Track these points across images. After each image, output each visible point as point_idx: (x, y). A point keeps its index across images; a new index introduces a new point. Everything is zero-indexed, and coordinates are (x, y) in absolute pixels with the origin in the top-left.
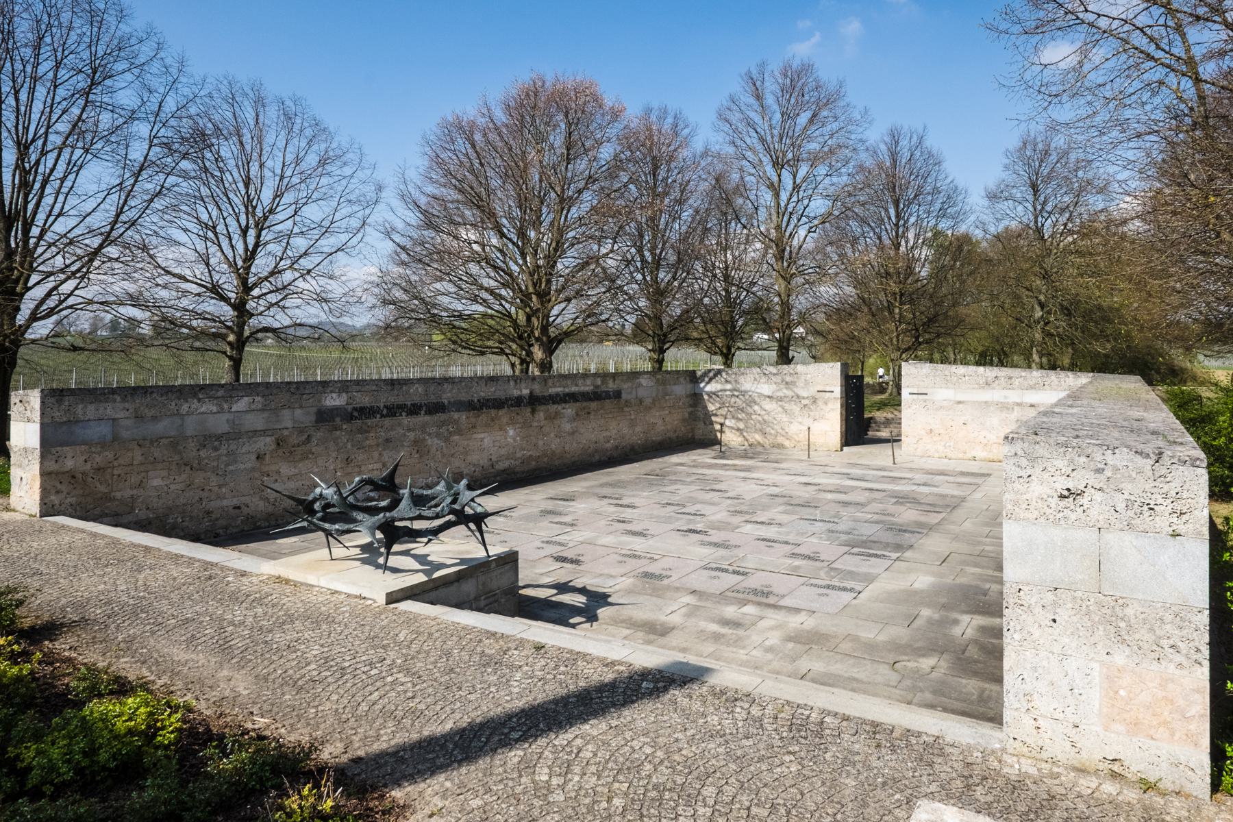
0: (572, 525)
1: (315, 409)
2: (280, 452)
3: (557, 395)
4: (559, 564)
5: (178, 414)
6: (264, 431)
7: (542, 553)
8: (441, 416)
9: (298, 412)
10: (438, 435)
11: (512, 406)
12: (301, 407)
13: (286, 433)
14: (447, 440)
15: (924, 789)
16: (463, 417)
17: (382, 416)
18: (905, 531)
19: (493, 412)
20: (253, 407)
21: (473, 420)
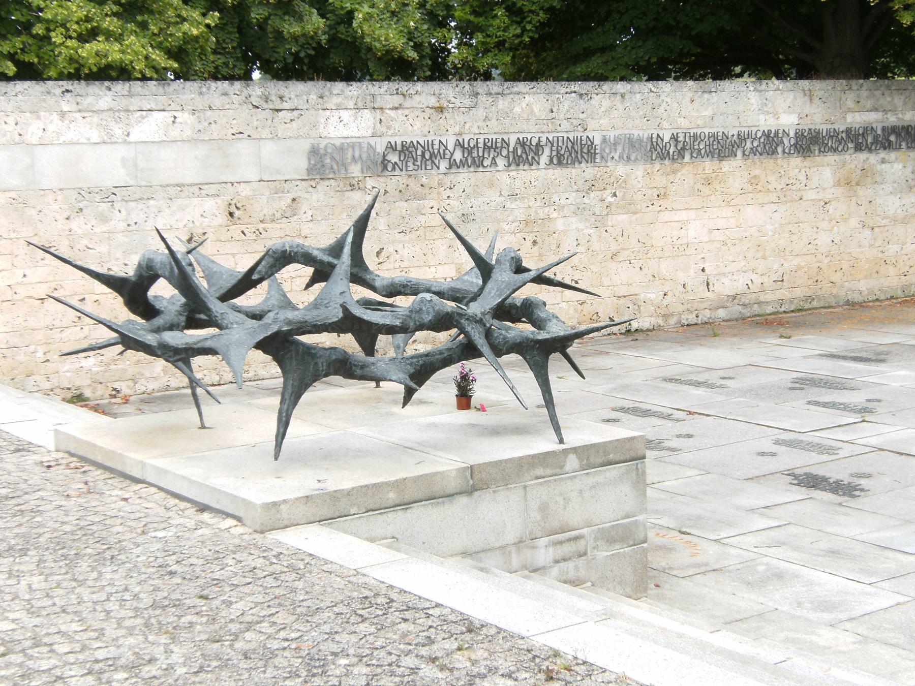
0: (865, 410)
1: (306, 145)
2: (236, 230)
3: (868, 130)
4: (801, 493)
5: (20, 142)
6: (200, 186)
7: (770, 465)
8: (584, 172)
9: (269, 148)
10: (579, 210)
11: (754, 151)
12: (275, 137)
13: (245, 191)
14: (599, 222)
15: (201, 562)
16: (638, 175)
17: (452, 165)
18: (883, 450)
19: (709, 165)
20: (174, 133)
21: (660, 180)
